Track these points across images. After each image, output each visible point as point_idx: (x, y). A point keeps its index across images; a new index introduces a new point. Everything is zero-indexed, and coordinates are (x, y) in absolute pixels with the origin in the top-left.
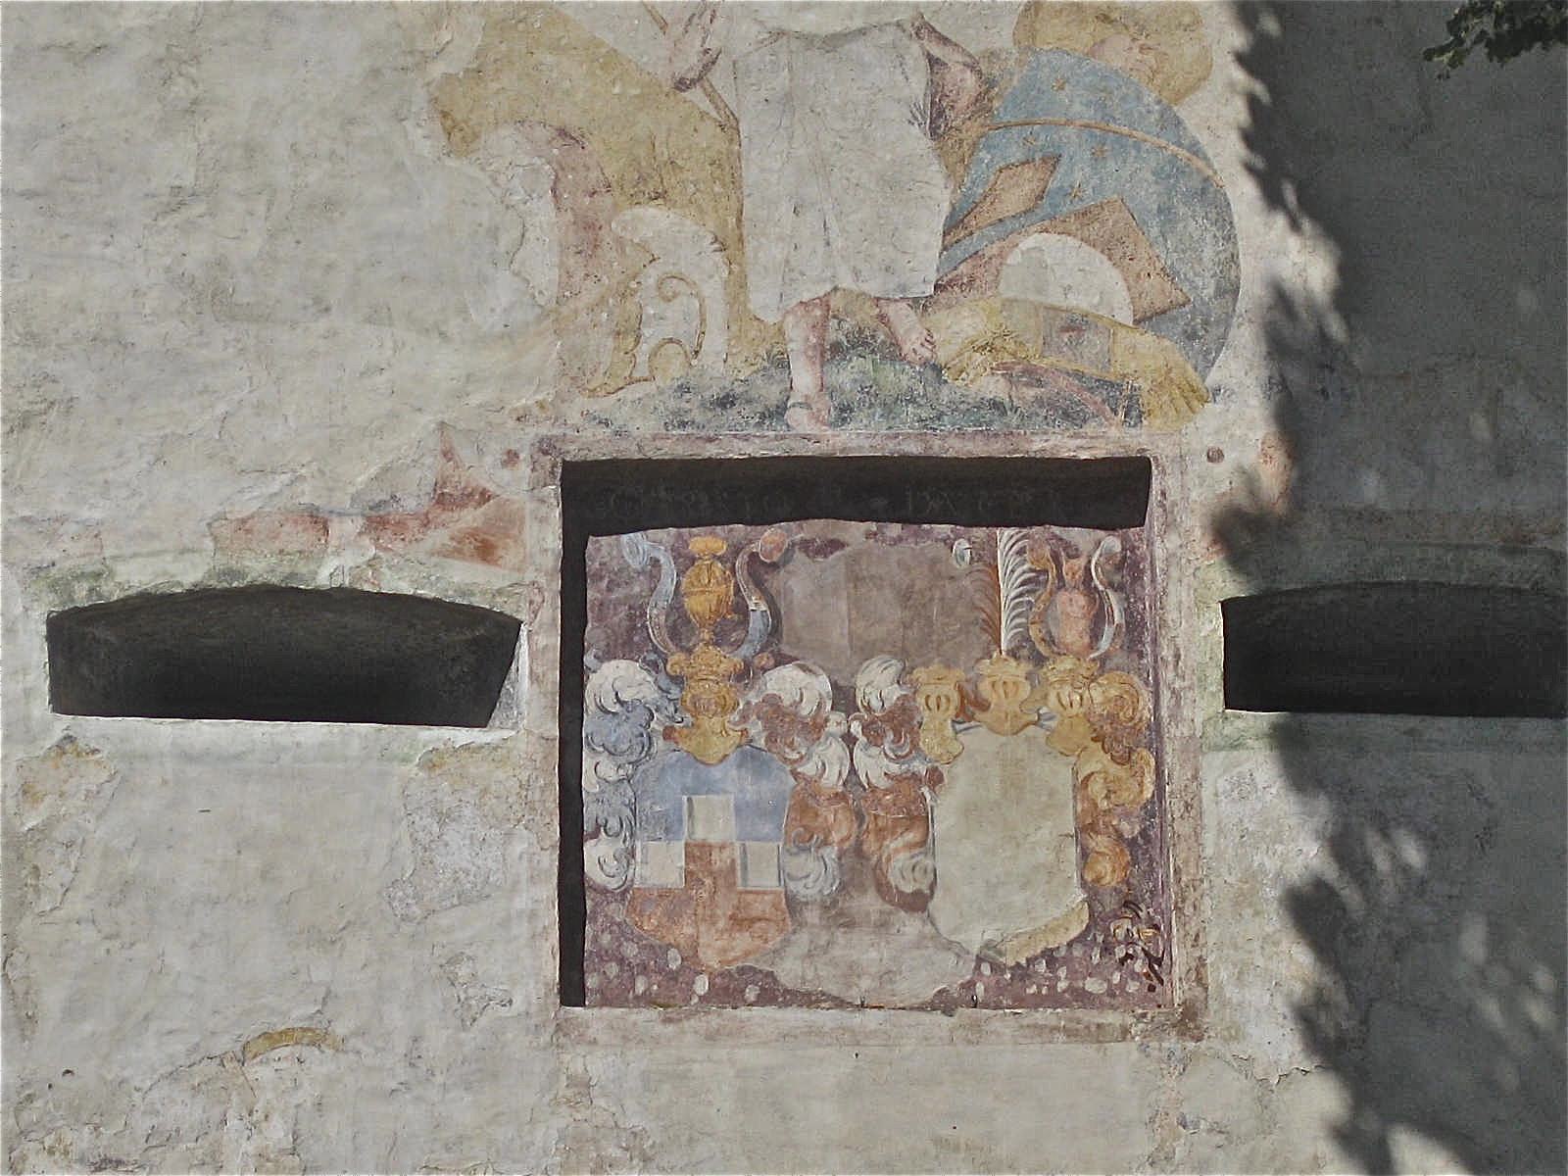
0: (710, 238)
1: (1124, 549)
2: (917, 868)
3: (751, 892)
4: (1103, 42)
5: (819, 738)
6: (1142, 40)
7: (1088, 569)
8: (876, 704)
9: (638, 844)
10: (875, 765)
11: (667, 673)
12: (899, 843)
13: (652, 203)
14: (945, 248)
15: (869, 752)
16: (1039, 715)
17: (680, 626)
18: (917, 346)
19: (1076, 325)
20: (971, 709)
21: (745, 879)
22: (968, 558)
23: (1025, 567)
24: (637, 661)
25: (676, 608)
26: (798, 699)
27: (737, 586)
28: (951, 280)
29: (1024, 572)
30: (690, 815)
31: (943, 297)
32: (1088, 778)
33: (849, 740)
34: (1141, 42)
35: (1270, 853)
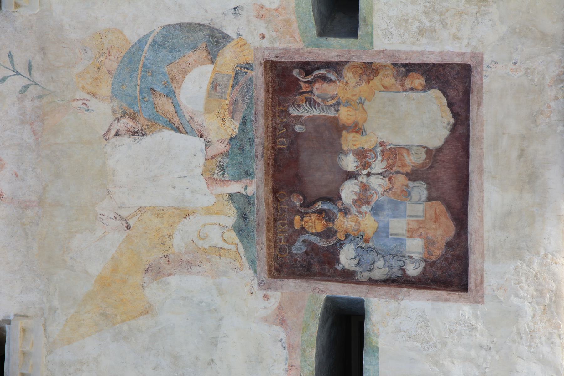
0: (185, 220)
1: (297, 68)
2: (417, 153)
3: (425, 215)
4: (108, 70)
5: (368, 186)
6: (106, 55)
7: (305, 82)
8: (356, 164)
9: (408, 255)
10: (378, 166)
11: (344, 240)
12: (407, 158)
13: (172, 240)
14: (187, 133)
15: (373, 168)
16: (360, 103)
17: (328, 233)
18: (223, 146)
19: (214, 85)
20: (357, 129)
21: (420, 216)
22: (301, 126)
23: (304, 105)
24: (340, 250)
25: (319, 235)
26: (354, 193)
27: (312, 213)
28: (199, 132)
29: (307, 106)
30: (396, 235)
31: (205, 136)
32: (384, 87)
33: (369, 175)
34: (107, 56)
35: (412, 24)
